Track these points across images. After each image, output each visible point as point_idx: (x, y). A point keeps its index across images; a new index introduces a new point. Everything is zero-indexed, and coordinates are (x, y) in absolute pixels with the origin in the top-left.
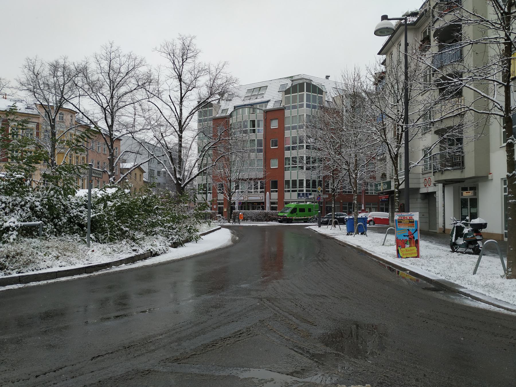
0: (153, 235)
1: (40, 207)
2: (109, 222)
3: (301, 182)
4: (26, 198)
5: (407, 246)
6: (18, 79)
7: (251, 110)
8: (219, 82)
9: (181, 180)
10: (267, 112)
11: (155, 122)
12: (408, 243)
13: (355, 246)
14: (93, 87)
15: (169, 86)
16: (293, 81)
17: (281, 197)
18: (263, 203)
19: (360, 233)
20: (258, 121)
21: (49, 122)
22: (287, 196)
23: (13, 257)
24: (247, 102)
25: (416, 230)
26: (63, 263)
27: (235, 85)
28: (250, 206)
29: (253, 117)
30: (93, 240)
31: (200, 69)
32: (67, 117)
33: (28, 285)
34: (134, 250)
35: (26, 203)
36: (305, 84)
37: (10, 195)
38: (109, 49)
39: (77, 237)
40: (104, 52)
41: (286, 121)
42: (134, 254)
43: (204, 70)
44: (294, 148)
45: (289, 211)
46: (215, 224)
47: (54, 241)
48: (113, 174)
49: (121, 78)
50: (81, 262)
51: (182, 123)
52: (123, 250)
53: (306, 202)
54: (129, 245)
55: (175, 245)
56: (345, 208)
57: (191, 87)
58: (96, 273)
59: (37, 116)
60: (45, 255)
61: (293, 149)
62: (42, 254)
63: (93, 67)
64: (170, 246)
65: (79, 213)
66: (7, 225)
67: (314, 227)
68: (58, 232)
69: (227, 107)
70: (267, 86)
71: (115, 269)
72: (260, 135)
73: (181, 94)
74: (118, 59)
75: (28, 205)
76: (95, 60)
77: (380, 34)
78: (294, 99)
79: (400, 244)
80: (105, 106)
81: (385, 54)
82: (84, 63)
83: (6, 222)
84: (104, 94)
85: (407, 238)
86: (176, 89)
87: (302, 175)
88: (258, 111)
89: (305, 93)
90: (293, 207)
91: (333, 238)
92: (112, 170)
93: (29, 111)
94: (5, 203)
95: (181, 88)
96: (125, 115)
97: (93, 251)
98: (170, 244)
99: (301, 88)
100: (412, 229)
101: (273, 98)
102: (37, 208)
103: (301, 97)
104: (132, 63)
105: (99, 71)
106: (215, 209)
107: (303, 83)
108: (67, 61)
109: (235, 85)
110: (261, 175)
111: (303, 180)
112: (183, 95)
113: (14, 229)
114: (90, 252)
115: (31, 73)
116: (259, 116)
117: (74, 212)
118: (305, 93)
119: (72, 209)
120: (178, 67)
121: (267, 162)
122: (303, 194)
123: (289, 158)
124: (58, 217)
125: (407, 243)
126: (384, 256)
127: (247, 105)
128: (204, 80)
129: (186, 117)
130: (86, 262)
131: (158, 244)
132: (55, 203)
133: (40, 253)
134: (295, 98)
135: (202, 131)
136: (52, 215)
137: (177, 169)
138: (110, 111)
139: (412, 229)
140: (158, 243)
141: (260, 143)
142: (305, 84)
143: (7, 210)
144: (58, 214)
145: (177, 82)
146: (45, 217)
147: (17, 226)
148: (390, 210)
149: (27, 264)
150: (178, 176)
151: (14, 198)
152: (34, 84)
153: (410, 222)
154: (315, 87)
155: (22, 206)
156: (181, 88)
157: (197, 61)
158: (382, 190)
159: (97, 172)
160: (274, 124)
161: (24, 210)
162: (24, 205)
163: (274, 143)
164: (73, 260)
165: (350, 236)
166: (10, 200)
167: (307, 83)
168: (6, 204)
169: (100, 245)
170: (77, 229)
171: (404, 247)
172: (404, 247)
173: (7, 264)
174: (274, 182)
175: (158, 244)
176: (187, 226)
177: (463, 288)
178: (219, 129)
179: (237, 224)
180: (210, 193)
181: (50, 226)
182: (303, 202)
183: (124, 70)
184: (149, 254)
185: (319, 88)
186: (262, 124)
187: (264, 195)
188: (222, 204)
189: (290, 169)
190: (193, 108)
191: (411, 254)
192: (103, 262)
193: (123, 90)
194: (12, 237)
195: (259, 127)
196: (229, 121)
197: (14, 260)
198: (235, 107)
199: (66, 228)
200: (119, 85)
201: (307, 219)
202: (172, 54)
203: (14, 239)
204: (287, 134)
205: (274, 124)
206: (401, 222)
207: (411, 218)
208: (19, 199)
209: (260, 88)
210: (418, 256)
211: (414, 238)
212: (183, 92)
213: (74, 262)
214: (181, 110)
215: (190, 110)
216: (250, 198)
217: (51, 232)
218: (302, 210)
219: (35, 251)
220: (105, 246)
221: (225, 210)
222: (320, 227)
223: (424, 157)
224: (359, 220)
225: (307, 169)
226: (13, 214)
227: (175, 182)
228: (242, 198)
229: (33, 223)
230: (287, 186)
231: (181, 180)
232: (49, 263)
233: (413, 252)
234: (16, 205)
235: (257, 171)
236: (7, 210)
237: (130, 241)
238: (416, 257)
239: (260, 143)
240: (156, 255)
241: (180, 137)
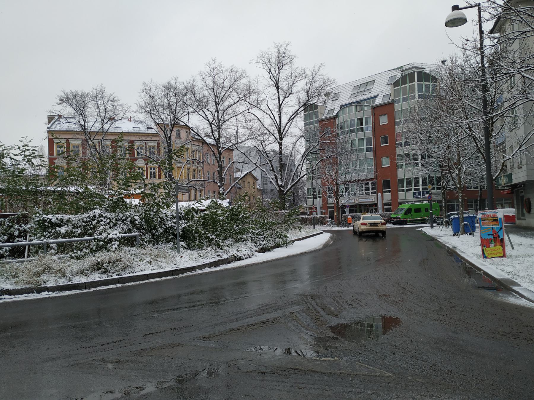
0: (243, 241)
1: (139, 221)
2: (197, 231)
3: (416, 179)
4: (127, 214)
5: (492, 245)
6: (137, 103)
7: (358, 107)
8: (317, 85)
9: (283, 187)
10: (375, 108)
11: (264, 128)
12: (493, 242)
13: (451, 247)
14: (201, 104)
15: (268, 95)
16: (402, 71)
17: (395, 197)
18: (376, 205)
19: (468, 233)
20: (366, 118)
21: (165, 140)
22: (402, 196)
23: (114, 263)
24: (354, 100)
25: (501, 228)
26: (154, 268)
27: (333, 86)
28: (362, 208)
29: (360, 115)
30: (184, 248)
31: (297, 74)
32: (183, 133)
33: (125, 285)
34: (218, 256)
35: (127, 218)
36: (416, 73)
37: (114, 212)
38: (212, 66)
39: (171, 245)
40: (208, 70)
41: (396, 116)
42: (217, 259)
43: (301, 75)
44: (406, 144)
45: (403, 212)
46: (318, 229)
47: (151, 249)
48: (223, 185)
49: (225, 92)
50: (169, 266)
51: (282, 131)
52: (209, 255)
53: (423, 201)
54: (213, 251)
55: (263, 250)
56: (471, 206)
57: (289, 93)
58: (181, 276)
59: (157, 135)
60: (140, 261)
61: (405, 145)
62: (137, 260)
63: (199, 84)
64: (256, 251)
65: (173, 224)
66: (110, 236)
67: (427, 229)
68: (156, 241)
69: (334, 106)
70: (374, 81)
71: (199, 272)
72: (369, 131)
73: (279, 101)
74: (221, 74)
75: (128, 220)
76: (200, 78)
77: (452, 25)
78: (404, 92)
79: (485, 243)
80: (211, 120)
81: (499, 31)
82: (192, 82)
83: (109, 234)
84: (210, 110)
85: (492, 237)
86: (273, 97)
87: (419, 173)
88: (366, 107)
89: (416, 83)
90: (407, 207)
91: (436, 240)
92: (221, 181)
93: (149, 131)
94: (109, 218)
95: (279, 96)
96: (229, 128)
97: (182, 257)
98: (257, 249)
99: (412, 77)
100: (496, 227)
101: (381, 92)
102: (137, 222)
103: (412, 89)
104: (234, 77)
105: (205, 88)
106: (324, 214)
107: (414, 73)
108: (177, 82)
109: (333, 86)
110: (372, 175)
111: (418, 178)
112: (281, 102)
113: (116, 240)
114: (179, 258)
115: (147, 96)
116: (367, 113)
117: (169, 223)
118: (416, 83)
119: (168, 220)
120: (275, 75)
122: (419, 193)
123: (401, 155)
124: (155, 228)
125: (493, 242)
126: (471, 257)
127: (354, 103)
128: (301, 85)
129: (285, 124)
130: (174, 266)
131: (244, 250)
132: (152, 216)
133: (136, 259)
134: (404, 90)
135: (307, 135)
136: (150, 227)
137: (279, 176)
138: (217, 125)
139: (496, 227)
140: (243, 249)
141: (368, 141)
142: (416, 73)
143: (111, 224)
144: (155, 226)
145: (274, 90)
146: (144, 229)
147: (118, 238)
148: (515, 206)
149: (124, 268)
150: (280, 183)
151: (117, 214)
152: (151, 107)
153: (494, 220)
154: (427, 75)
155: (123, 220)
156: (279, 96)
157: (294, 67)
158: (503, 183)
159: (183, 188)
160: (384, 120)
161: (125, 224)
162: (126, 220)
163: (384, 140)
164: (163, 264)
165: (456, 237)
166: (114, 216)
167: (418, 72)
168: (110, 220)
169: (189, 252)
170: (172, 238)
171: (489, 247)
172: (489, 247)
173: (109, 269)
174: (386, 182)
175: (244, 250)
176: (277, 232)
177: (519, 285)
178: (325, 131)
179: (346, 228)
180: (320, 197)
181: (148, 236)
182: (419, 201)
183: (227, 84)
184: (233, 259)
185: (432, 76)
186: (370, 121)
187: (376, 197)
188: (333, 207)
189: (404, 166)
190: (291, 114)
191: (496, 254)
192: (189, 266)
193: (226, 104)
194: (114, 247)
195: (367, 124)
196: (335, 122)
197: (115, 265)
198: (341, 106)
199: (163, 237)
200: (223, 99)
201: (425, 220)
202: (268, 64)
203: (116, 248)
204: (398, 129)
205: (384, 120)
206: (485, 220)
207: (495, 215)
208: (121, 215)
209: (367, 83)
210: (504, 256)
211: (499, 236)
212: (281, 99)
213: (164, 266)
214: (280, 117)
215: (289, 117)
217: (149, 242)
218: (418, 210)
219: (133, 257)
220: (192, 252)
221: (336, 214)
222: (432, 227)
223: (520, 148)
224: (464, 219)
225: (422, 166)
226: (116, 228)
227: (278, 189)
228: (353, 201)
229: (133, 234)
230: (400, 185)
231: (283, 187)
232: (143, 267)
233: (498, 251)
234: (119, 220)
235: (366, 170)
236: (111, 224)
237: (215, 247)
238: (502, 257)
239: (368, 141)
240: (240, 259)
241: (281, 145)
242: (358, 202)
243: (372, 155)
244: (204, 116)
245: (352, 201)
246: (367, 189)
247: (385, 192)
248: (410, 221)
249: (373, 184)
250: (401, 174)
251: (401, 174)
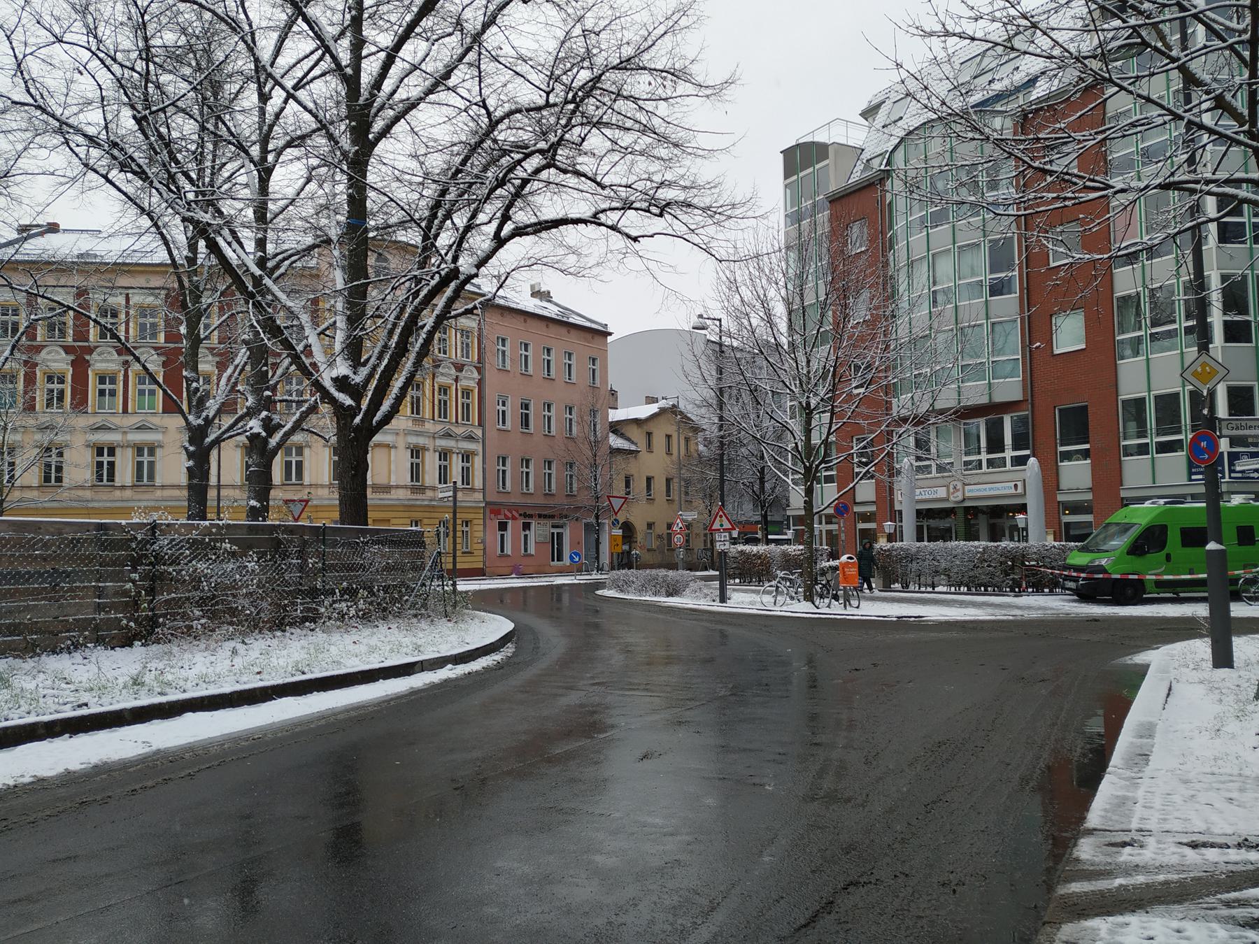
22: (1135, 471)
45: (1120, 543)
110: (1010, 388)
121: (1036, 329)
216: (972, 491)
228: (942, 493)
242: (959, 496)
243: (1015, 307)
244: (309, 77)
245: (936, 492)
246: (996, 444)
247: (1067, 456)
248: (1160, 585)
249: (1019, 424)
250: (1133, 379)
251: (1133, 379)
